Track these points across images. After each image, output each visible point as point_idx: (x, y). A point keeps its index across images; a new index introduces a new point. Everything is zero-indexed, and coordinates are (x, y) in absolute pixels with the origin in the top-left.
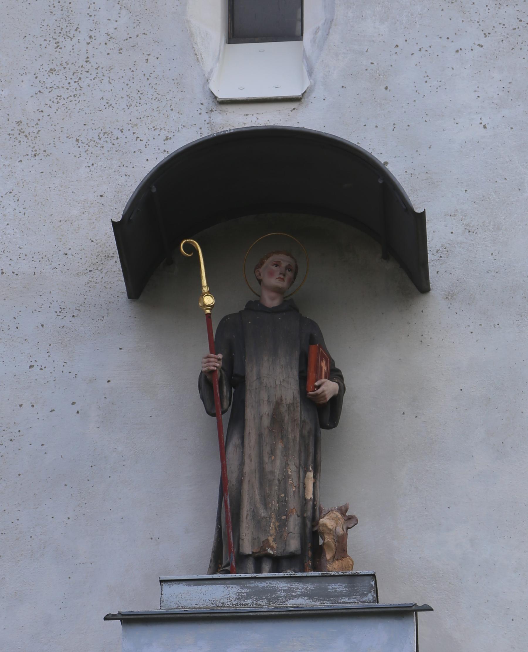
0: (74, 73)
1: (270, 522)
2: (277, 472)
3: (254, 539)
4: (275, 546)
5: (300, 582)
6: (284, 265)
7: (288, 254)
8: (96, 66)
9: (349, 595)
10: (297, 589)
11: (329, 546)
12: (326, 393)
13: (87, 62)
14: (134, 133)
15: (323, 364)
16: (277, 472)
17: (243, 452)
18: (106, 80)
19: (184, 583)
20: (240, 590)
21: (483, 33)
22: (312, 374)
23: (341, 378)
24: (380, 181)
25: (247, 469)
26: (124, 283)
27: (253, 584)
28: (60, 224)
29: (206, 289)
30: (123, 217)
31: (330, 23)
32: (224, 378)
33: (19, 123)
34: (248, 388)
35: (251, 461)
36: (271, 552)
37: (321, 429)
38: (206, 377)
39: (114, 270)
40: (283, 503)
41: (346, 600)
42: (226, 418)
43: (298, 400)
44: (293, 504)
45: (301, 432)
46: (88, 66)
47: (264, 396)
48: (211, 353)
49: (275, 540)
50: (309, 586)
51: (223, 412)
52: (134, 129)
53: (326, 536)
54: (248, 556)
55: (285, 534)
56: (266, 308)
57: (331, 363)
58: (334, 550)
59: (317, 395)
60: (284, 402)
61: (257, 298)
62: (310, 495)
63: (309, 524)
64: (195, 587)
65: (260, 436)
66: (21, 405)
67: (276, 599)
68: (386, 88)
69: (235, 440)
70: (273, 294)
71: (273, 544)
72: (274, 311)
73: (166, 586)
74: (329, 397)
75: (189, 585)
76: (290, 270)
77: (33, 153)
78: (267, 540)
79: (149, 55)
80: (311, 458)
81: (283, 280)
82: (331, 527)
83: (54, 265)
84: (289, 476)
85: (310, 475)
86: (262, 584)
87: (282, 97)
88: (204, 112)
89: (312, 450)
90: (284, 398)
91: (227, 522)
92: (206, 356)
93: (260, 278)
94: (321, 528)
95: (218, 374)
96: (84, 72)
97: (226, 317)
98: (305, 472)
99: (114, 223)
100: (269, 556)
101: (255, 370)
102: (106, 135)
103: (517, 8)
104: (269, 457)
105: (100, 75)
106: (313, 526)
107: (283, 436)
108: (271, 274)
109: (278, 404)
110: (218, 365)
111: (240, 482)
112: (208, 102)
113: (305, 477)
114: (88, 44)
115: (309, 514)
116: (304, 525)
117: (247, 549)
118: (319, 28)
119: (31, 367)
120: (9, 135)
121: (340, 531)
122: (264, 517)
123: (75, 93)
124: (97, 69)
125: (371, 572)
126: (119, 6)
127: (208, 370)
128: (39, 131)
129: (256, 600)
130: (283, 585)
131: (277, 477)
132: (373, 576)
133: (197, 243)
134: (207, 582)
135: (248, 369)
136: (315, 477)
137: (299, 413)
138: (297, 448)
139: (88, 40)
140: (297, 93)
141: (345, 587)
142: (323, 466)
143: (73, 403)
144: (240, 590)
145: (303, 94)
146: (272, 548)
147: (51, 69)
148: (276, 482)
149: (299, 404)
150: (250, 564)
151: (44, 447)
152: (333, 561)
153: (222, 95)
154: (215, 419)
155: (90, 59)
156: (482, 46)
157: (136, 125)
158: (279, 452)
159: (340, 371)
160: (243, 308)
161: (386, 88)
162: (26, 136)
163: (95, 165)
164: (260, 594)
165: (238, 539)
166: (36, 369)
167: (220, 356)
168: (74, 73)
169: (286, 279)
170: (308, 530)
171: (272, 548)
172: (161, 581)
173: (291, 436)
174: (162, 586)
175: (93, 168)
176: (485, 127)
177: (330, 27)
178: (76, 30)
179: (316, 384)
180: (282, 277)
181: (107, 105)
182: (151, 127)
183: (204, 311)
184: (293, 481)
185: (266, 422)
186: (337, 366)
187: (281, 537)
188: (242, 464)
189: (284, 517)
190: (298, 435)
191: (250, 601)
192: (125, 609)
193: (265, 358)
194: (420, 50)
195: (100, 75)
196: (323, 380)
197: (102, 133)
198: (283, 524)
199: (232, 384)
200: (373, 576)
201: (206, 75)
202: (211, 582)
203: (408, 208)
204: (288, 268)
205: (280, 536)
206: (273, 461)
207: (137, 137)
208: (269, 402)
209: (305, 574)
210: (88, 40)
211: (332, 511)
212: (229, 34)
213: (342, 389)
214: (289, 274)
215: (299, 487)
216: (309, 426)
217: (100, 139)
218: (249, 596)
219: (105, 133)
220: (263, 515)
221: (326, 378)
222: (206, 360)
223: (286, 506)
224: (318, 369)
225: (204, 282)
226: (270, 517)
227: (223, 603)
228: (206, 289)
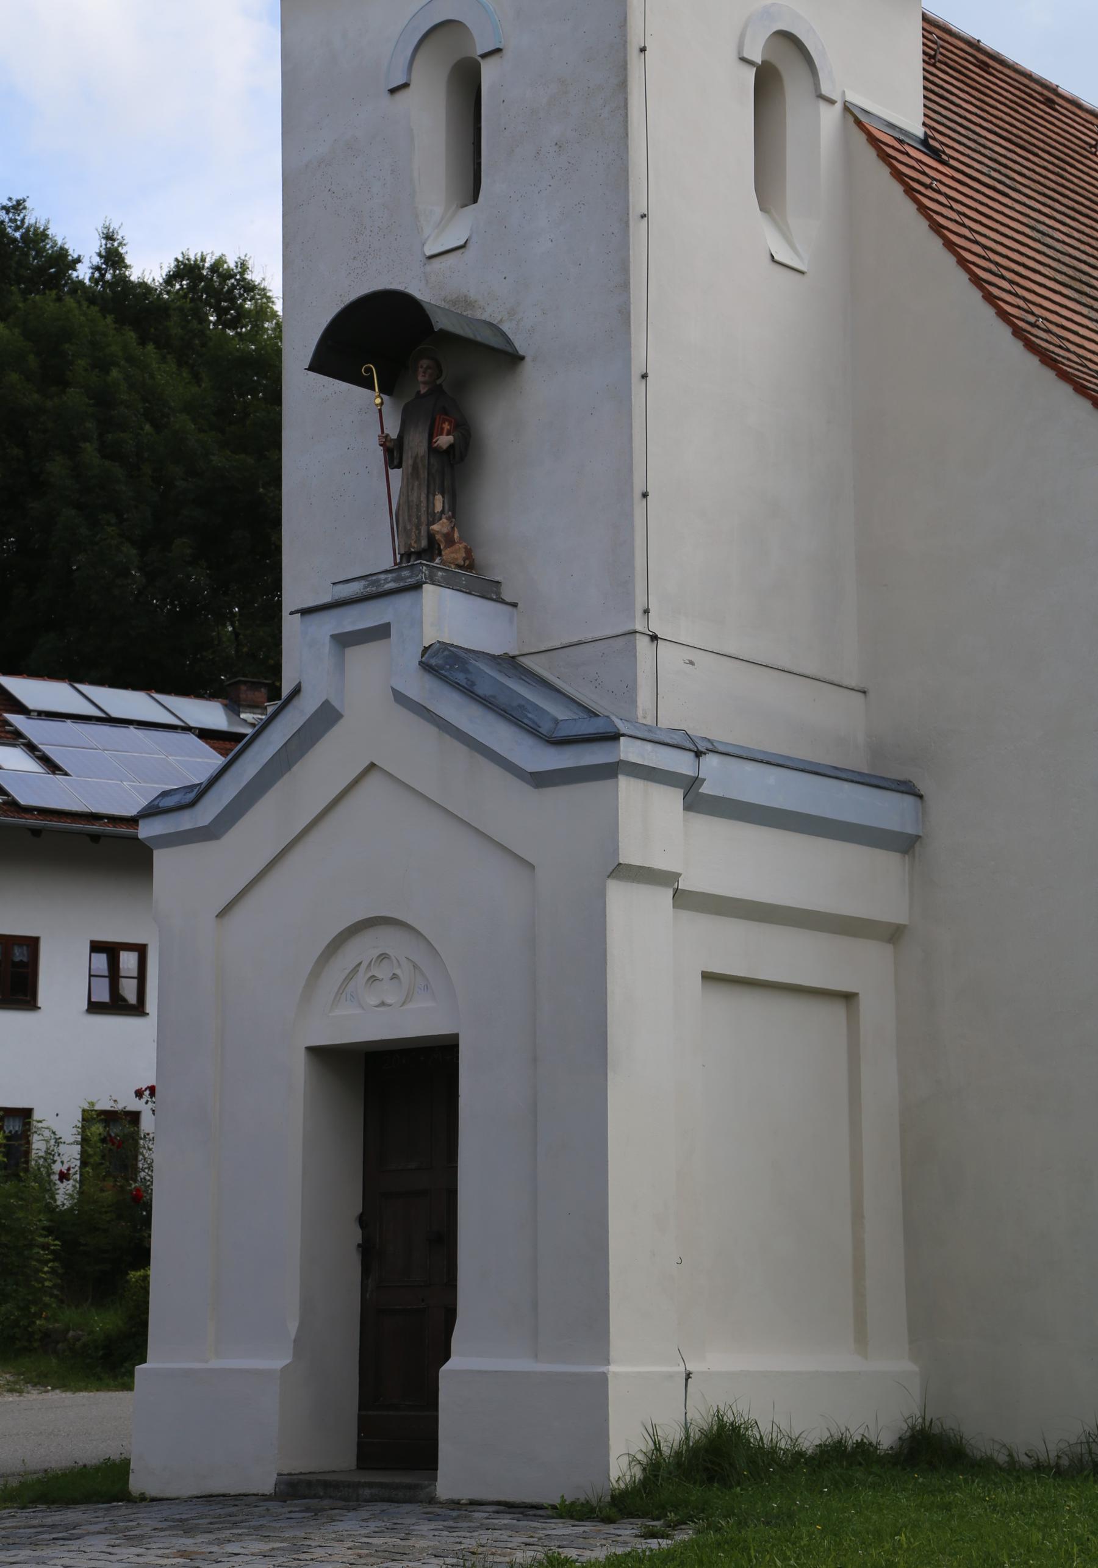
5: (390, 573)
16: (415, 500)
20: (365, 583)
40: (419, 518)
41: (410, 580)
49: (415, 542)
50: (394, 575)
67: (379, 586)
87: (1025, 68)
100: (412, 552)
109: (416, 457)
140: (462, 242)
144: (365, 583)
146: (414, 548)
158: (415, 488)
171: (414, 548)
184: (424, 504)
192: (300, 607)
205: (418, 540)
218: (368, 586)
226: (412, 529)
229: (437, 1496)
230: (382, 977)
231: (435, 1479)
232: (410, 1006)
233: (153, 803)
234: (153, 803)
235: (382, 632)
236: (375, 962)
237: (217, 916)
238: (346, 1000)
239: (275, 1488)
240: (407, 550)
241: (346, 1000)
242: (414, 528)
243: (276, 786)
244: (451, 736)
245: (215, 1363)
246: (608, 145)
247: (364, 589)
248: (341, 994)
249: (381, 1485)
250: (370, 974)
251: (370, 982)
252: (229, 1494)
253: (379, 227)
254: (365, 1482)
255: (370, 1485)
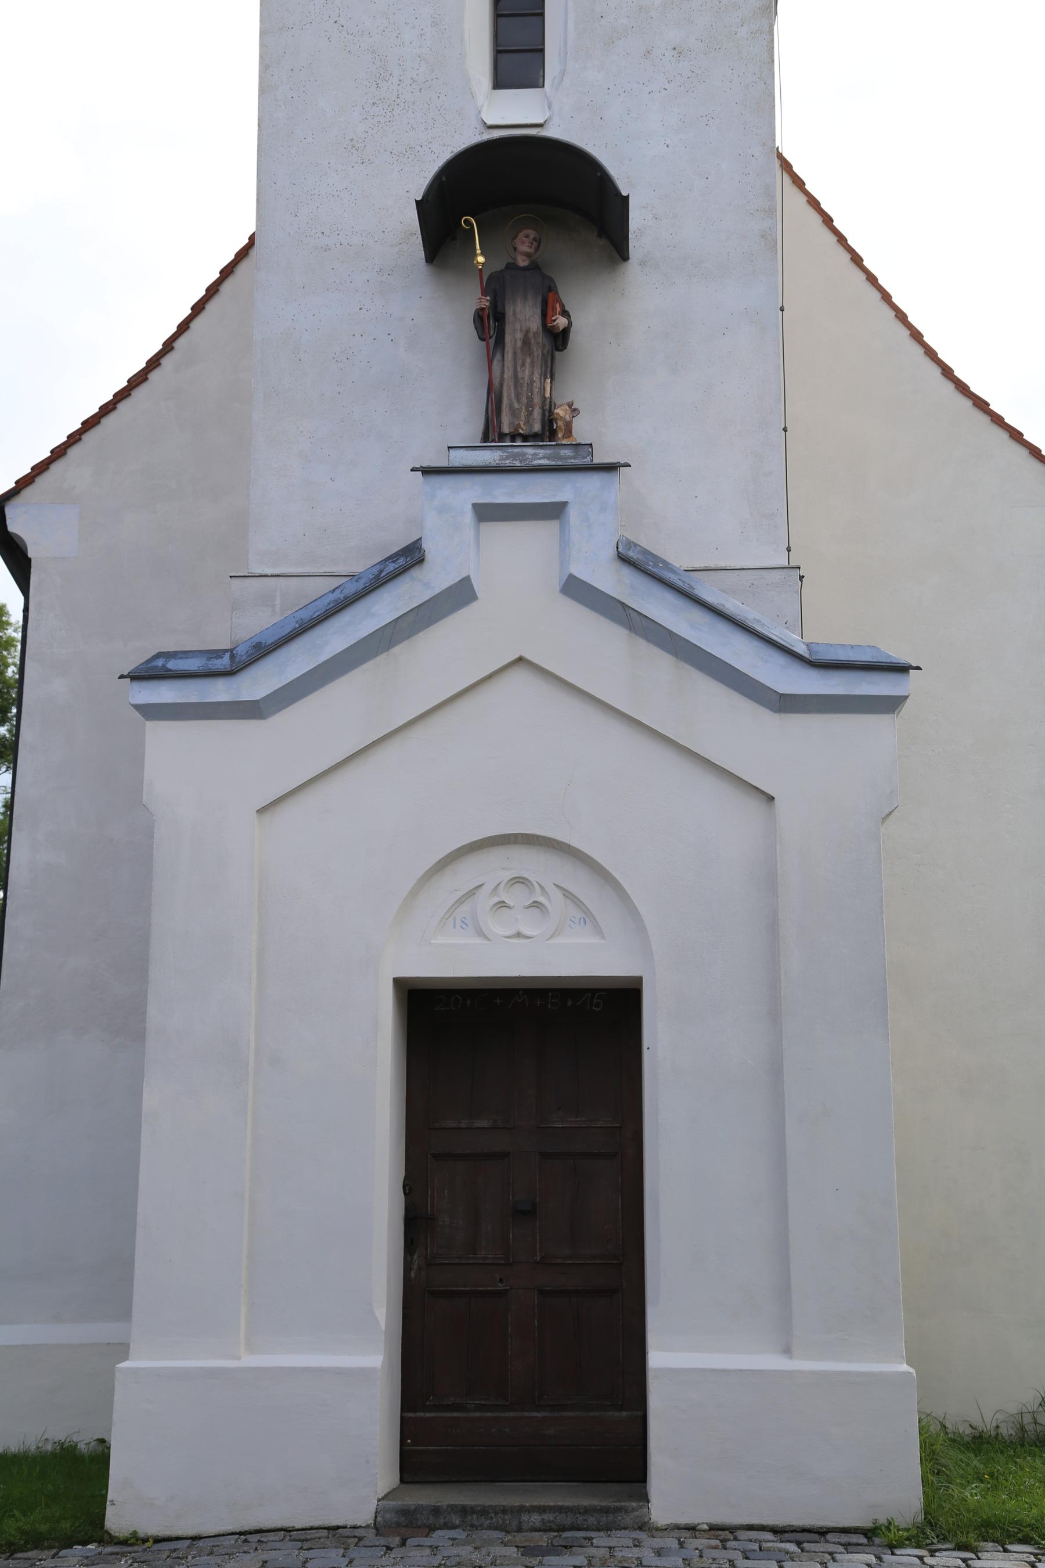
0: (389, 106)
1: (521, 412)
2: (526, 378)
3: (510, 423)
4: (524, 428)
5: (541, 449)
6: (532, 236)
7: (534, 230)
8: (404, 101)
9: (574, 458)
10: (539, 453)
11: (560, 428)
12: (559, 325)
13: (398, 98)
14: (430, 148)
15: (558, 306)
16: (526, 378)
17: (503, 365)
18: (411, 111)
19: (464, 449)
20: (501, 454)
21: (667, 80)
22: (550, 312)
23: (569, 316)
24: (599, 174)
25: (506, 376)
26: (423, 252)
27: (510, 450)
28: (379, 211)
29: (479, 252)
30: (423, 197)
31: (563, 72)
32: (490, 314)
33: (352, 140)
34: (507, 321)
35: (509, 370)
36: (522, 432)
37: (556, 352)
38: (478, 313)
39: (416, 243)
40: (530, 399)
41: (573, 461)
42: (492, 341)
43: (541, 329)
44: (537, 400)
45: (542, 351)
46: (398, 101)
47: (518, 326)
48: (482, 295)
49: (524, 424)
50: (548, 452)
51: (490, 338)
52: (430, 145)
53: (559, 421)
54: (507, 434)
55: (531, 420)
56: (520, 267)
57: (562, 306)
58: (564, 432)
59: (553, 326)
60: (531, 330)
61: (513, 261)
62: (548, 395)
63: (547, 414)
64: (472, 452)
65: (515, 353)
66: (354, 335)
68: (601, 118)
69: (498, 357)
70: (524, 258)
71: (523, 426)
72: (525, 269)
73: (451, 450)
74: (561, 328)
75: (468, 450)
76: (536, 241)
77: (362, 161)
78: (519, 424)
79: (440, 93)
80: (549, 370)
81: (531, 247)
82: (561, 415)
83: (376, 239)
84: (534, 381)
85: (548, 381)
86: (516, 450)
88: (477, 134)
89: (549, 364)
90: (531, 328)
91: (492, 411)
92: (479, 297)
93: (515, 246)
94: (555, 416)
95: (487, 311)
96: (396, 106)
97: (491, 274)
98: (545, 380)
99: (416, 201)
100: (520, 435)
101: (512, 310)
102: (411, 149)
103: (691, 63)
104: (521, 368)
105: (407, 107)
106: (550, 416)
107: (531, 354)
108: (523, 243)
109: (528, 331)
110: (487, 304)
111: (501, 385)
112: (480, 127)
113: (544, 382)
114: (398, 85)
115: (547, 407)
116: (543, 415)
117: (506, 430)
118: (555, 77)
119: (360, 309)
120: (345, 148)
121: (568, 418)
122: (517, 409)
123: (390, 119)
124: (404, 103)
125: (590, 443)
126: (419, 59)
127: (480, 307)
128: (365, 146)
129: (512, 461)
130: (530, 451)
131: (526, 382)
132: (591, 445)
133: (472, 219)
134: (479, 448)
135: (507, 308)
136: (551, 383)
137: (541, 338)
138: (540, 362)
139: (399, 83)
140: (541, 121)
141: (572, 452)
142: (556, 376)
143: (389, 334)
144: (501, 454)
145: (545, 122)
147: (373, 103)
148: (526, 385)
149: (541, 333)
150: (508, 438)
151: (369, 364)
152: (563, 439)
153: (489, 122)
154: (484, 343)
155: (400, 96)
156: (666, 90)
157: (431, 142)
159: (568, 312)
160: (503, 268)
161: (601, 118)
162: (356, 149)
163: (403, 170)
164: (515, 456)
165: (500, 423)
166: (364, 310)
167: (488, 298)
168: (389, 106)
169: (533, 247)
170: (546, 418)
171: (522, 429)
172: (449, 448)
173: (536, 354)
174: (449, 451)
175: (401, 172)
176: (668, 146)
177: (563, 76)
178: (390, 75)
179: (553, 318)
180: (530, 245)
181: (411, 129)
182: (441, 143)
183: (477, 267)
185: (519, 344)
186: (566, 309)
187: (528, 422)
188: (503, 372)
189: (530, 409)
190: (540, 353)
191: (508, 461)
193: (519, 301)
194: (625, 92)
195: (407, 107)
196: (558, 316)
197: (408, 148)
198: (530, 414)
199: (496, 320)
200: (591, 445)
201: (479, 108)
202: (483, 448)
203: (618, 193)
204: (535, 239)
205: (528, 422)
206: (524, 371)
207: (432, 151)
208: (521, 330)
209: (545, 443)
210: (399, 83)
211: (563, 405)
212: (494, 84)
213: (570, 324)
214: (535, 244)
215: (541, 389)
216: (548, 348)
217: (407, 152)
218: (507, 458)
219: (410, 148)
220: (516, 407)
221: (559, 314)
222: (479, 301)
223: (532, 401)
224: (554, 309)
225: (478, 247)
227: (490, 463)
228: (479, 252)
229: (652, 1521)
230: (514, 904)
231: (645, 1498)
232: (559, 940)
233: (154, 664)
234: (154, 664)
235: (554, 511)
236: (507, 884)
237: (258, 811)
238: (455, 927)
239: (376, 1517)
240: (512, 430)
241: (455, 927)
242: (523, 407)
243: (365, 666)
244: (648, 640)
245: (250, 1361)
246: (746, 65)
247: (500, 460)
248: (447, 919)
249: (560, 1509)
250: (496, 899)
251: (495, 909)
252: (294, 1527)
253: (412, 79)
254: (532, 1507)
255: (541, 1510)
